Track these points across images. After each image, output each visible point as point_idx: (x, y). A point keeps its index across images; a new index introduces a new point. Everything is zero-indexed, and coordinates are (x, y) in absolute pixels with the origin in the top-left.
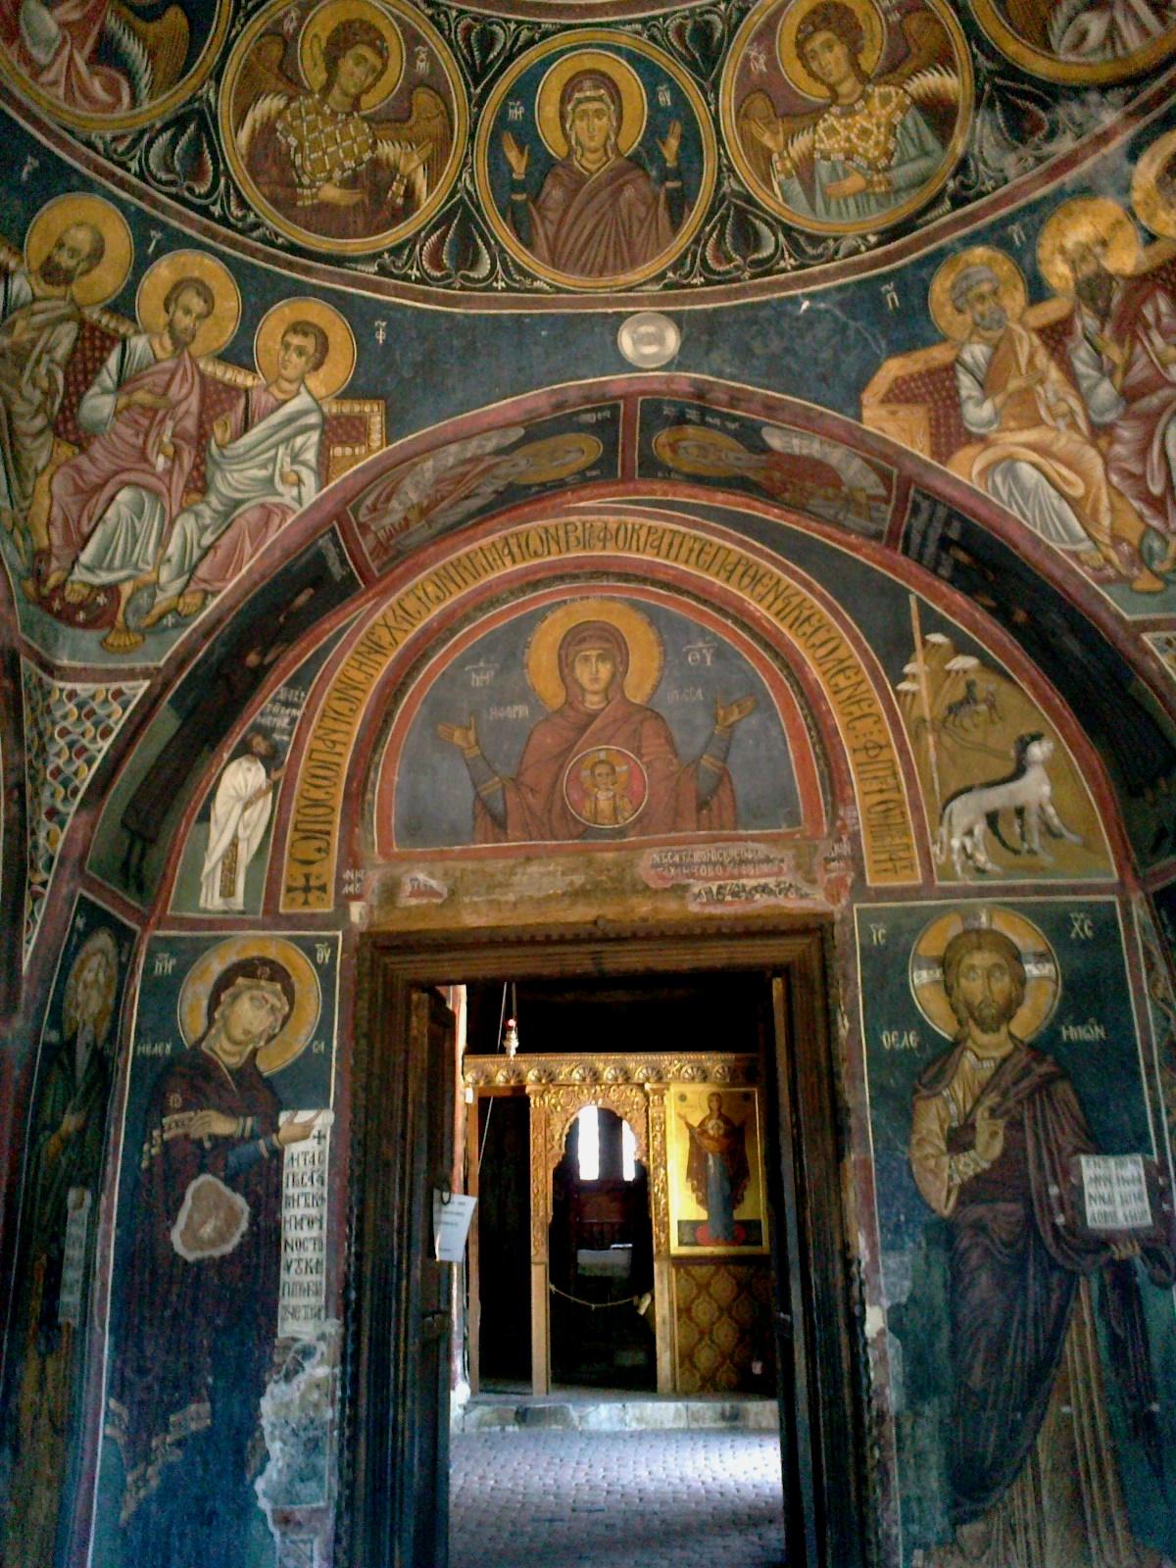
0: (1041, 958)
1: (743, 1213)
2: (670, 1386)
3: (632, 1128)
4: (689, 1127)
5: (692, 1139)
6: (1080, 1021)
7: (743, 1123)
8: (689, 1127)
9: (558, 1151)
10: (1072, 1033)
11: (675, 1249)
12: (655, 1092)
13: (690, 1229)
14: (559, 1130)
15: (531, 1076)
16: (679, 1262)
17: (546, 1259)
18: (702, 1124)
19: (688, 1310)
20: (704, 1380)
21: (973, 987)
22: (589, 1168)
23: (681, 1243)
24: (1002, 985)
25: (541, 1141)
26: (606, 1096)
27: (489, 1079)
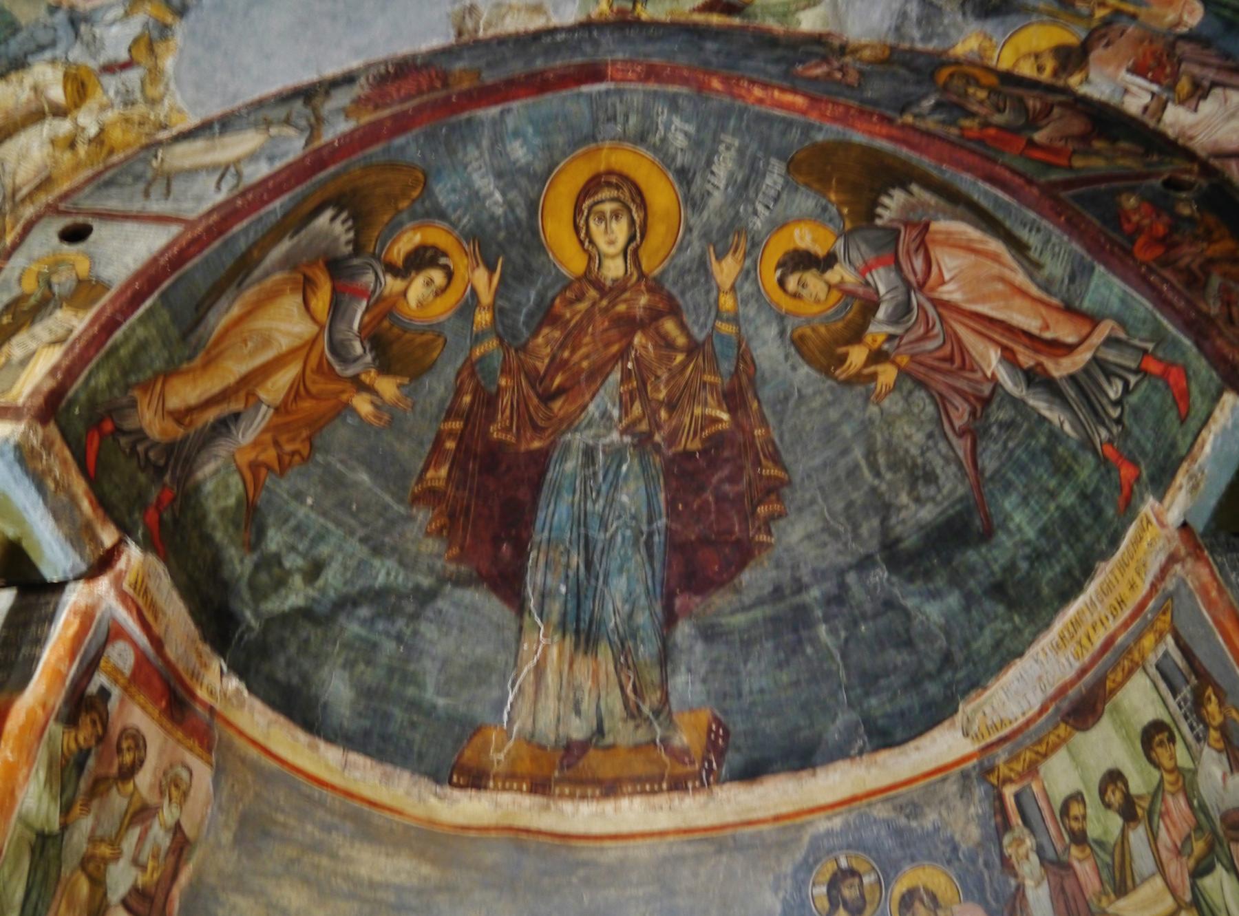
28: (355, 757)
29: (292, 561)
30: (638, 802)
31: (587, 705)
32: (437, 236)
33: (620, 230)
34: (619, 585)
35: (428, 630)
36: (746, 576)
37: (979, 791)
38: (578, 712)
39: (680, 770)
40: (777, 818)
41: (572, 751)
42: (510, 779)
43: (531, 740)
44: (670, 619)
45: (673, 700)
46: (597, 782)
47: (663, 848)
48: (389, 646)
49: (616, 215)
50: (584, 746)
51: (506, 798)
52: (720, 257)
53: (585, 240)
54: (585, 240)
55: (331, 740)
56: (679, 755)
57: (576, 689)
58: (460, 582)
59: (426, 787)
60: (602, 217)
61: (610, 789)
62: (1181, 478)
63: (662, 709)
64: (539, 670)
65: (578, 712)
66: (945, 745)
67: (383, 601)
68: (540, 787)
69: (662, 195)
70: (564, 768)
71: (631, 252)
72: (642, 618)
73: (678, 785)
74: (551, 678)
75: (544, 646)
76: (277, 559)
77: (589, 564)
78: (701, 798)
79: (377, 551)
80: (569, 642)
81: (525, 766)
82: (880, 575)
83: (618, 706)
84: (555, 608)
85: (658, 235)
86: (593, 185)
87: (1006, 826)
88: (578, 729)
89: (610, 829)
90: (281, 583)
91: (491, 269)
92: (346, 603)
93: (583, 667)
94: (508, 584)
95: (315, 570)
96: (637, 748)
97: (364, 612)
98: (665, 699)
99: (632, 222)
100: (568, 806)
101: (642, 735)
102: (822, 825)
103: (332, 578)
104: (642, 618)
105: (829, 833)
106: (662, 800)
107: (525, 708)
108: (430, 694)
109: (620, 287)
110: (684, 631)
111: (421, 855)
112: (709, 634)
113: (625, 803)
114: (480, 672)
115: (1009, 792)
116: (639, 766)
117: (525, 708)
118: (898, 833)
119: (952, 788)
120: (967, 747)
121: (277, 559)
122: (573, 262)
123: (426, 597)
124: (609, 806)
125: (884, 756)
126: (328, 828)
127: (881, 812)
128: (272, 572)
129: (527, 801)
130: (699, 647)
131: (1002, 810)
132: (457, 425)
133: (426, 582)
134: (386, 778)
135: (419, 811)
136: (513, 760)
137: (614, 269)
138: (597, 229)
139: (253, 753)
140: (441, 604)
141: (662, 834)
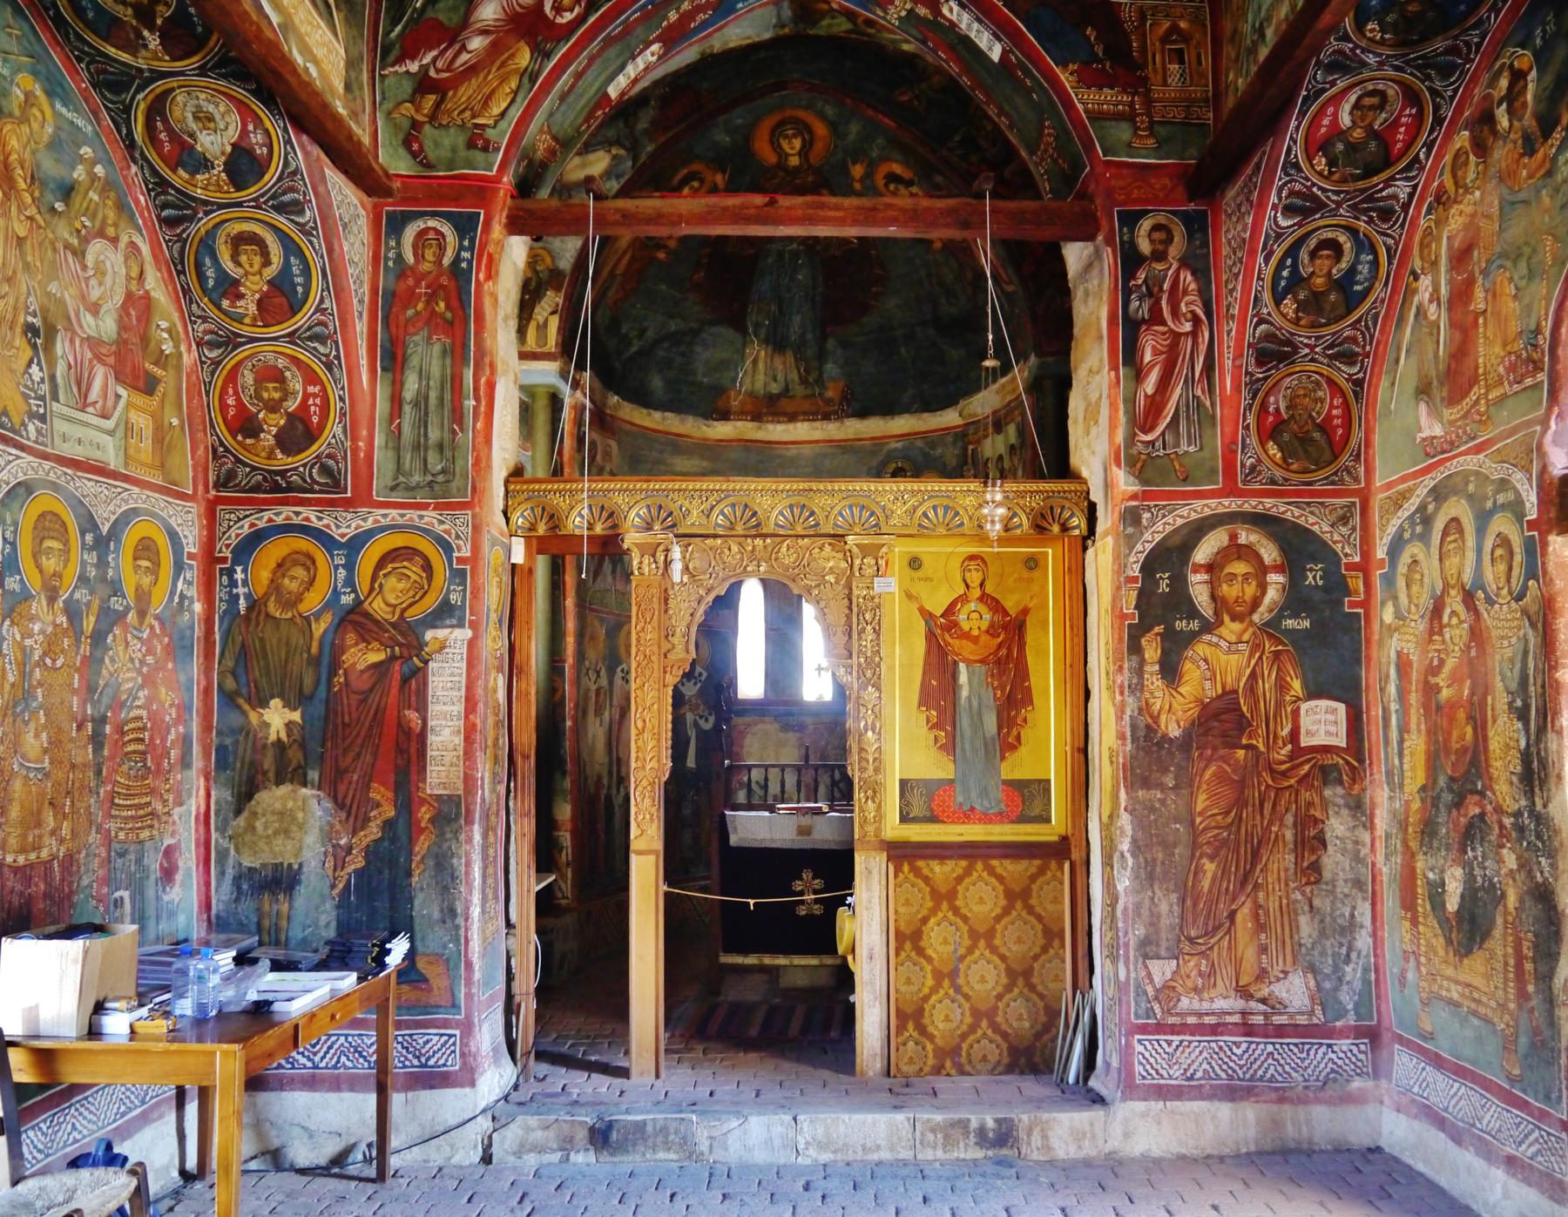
0: (1278, 569)
1: (1017, 767)
2: (878, 1065)
3: (822, 615)
4: (927, 615)
5: (931, 636)
6: (1295, 616)
7: (1025, 612)
8: (927, 615)
9: (682, 652)
10: (1290, 623)
11: (893, 828)
12: (866, 551)
13: (922, 799)
14: (686, 612)
15: (634, 516)
16: (901, 853)
17: (659, 845)
18: (950, 610)
19: (916, 936)
20: (941, 1053)
21: (1229, 591)
22: (750, 683)
23: (904, 819)
24: (1251, 590)
25: (650, 635)
26: (772, 556)
27: (554, 520)
28: (667, 414)
29: (634, 333)
30: (806, 424)
31: (780, 377)
32: (695, 167)
33: (797, 143)
34: (797, 319)
35: (698, 349)
36: (865, 319)
37: (960, 444)
38: (775, 380)
39: (829, 409)
40: (873, 438)
41: (772, 400)
42: (742, 415)
43: (751, 394)
44: (824, 338)
45: (825, 376)
46: (785, 414)
47: (817, 448)
48: (679, 360)
49: (795, 136)
50: (778, 397)
51: (739, 424)
52: (854, 163)
53: (777, 148)
54: (777, 148)
55: (656, 409)
56: (828, 401)
57: (774, 369)
58: (713, 323)
59: (701, 421)
60: (786, 137)
61: (792, 418)
62: (253, 996)
63: (820, 381)
64: (755, 362)
65: (775, 380)
66: (950, 418)
67: (675, 338)
68: (757, 417)
69: (820, 129)
70: (768, 407)
71: (804, 152)
72: (809, 336)
73: (826, 417)
74: (761, 365)
75: (757, 352)
76: (626, 335)
77: (781, 311)
78: (837, 424)
79: (672, 317)
80: (770, 349)
81: (749, 407)
82: (931, 331)
83: (796, 378)
84: (763, 333)
85: (819, 146)
86: (781, 124)
87: (966, 463)
88: (775, 388)
89: (792, 439)
90: (629, 345)
91: (724, 172)
92: (657, 343)
93: (778, 363)
94: (738, 323)
95: (643, 331)
96: (806, 397)
97: (666, 345)
98: (821, 375)
99: (804, 140)
100: (770, 427)
101: (809, 392)
102: (895, 445)
103: (650, 334)
104: (809, 336)
105: (895, 450)
106: (817, 424)
107: (748, 380)
108: (699, 377)
109: (797, 169)
110: (831, 344)
111: (702, 457)
112: (844, 344)
113: (799, 425)
114: (725, 365)
115: (971, 447)
116: (807, 406)
117: (748, 380)
118: (925, 455)
119: (950, 439)
120: (960, 422)
121: (626, 335)
122: (772, 159)
123: (696, 333)
124: (791, 426)
125: (925, 415)
126: (662, 452)
127: (919, 443)
128: (626, 341)
129: (750, 425)
130: (839, 351)
131: (966, 455)
132: (708, 250)
133: (694, 325)
134: (682, 421)
135: (698, 434)
136: (743, 404)
137: (794, 161)
138: (785, 144)
139: (628, 427)
140: (704, 335)
141: (817, 442)
